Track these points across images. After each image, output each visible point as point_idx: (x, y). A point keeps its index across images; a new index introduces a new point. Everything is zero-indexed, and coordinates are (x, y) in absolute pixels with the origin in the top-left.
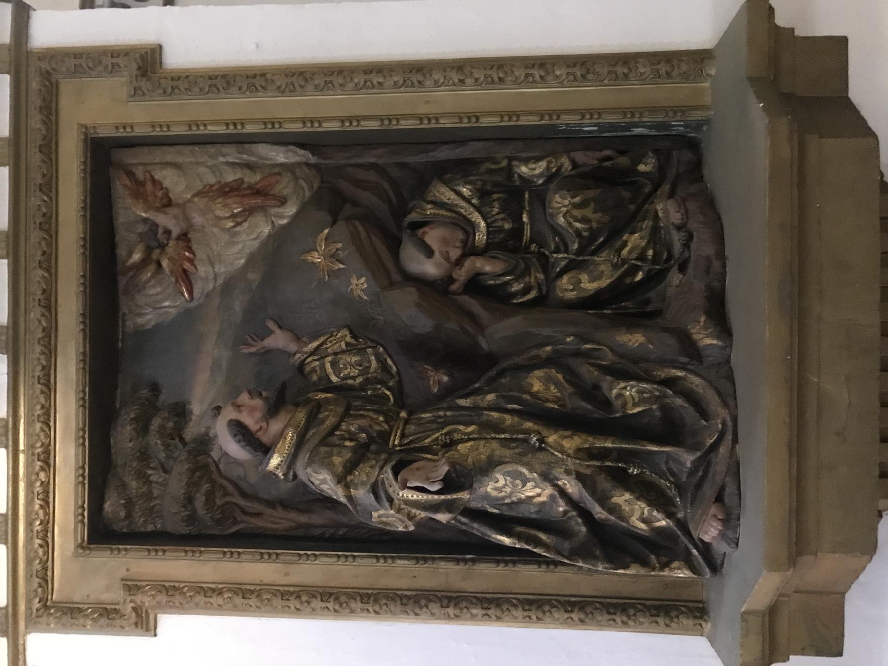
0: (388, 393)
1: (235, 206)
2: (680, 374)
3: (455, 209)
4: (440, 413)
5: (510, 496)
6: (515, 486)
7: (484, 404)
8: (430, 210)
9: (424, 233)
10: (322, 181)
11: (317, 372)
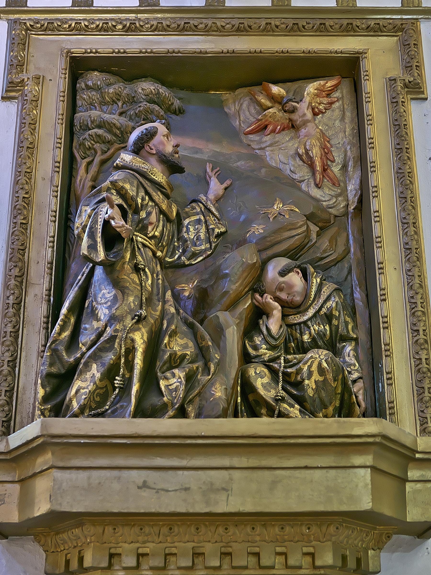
0: (176, 257)
4: (160, 276)
6: (106, 303)
8: (316, 281)
10: (336, 216)
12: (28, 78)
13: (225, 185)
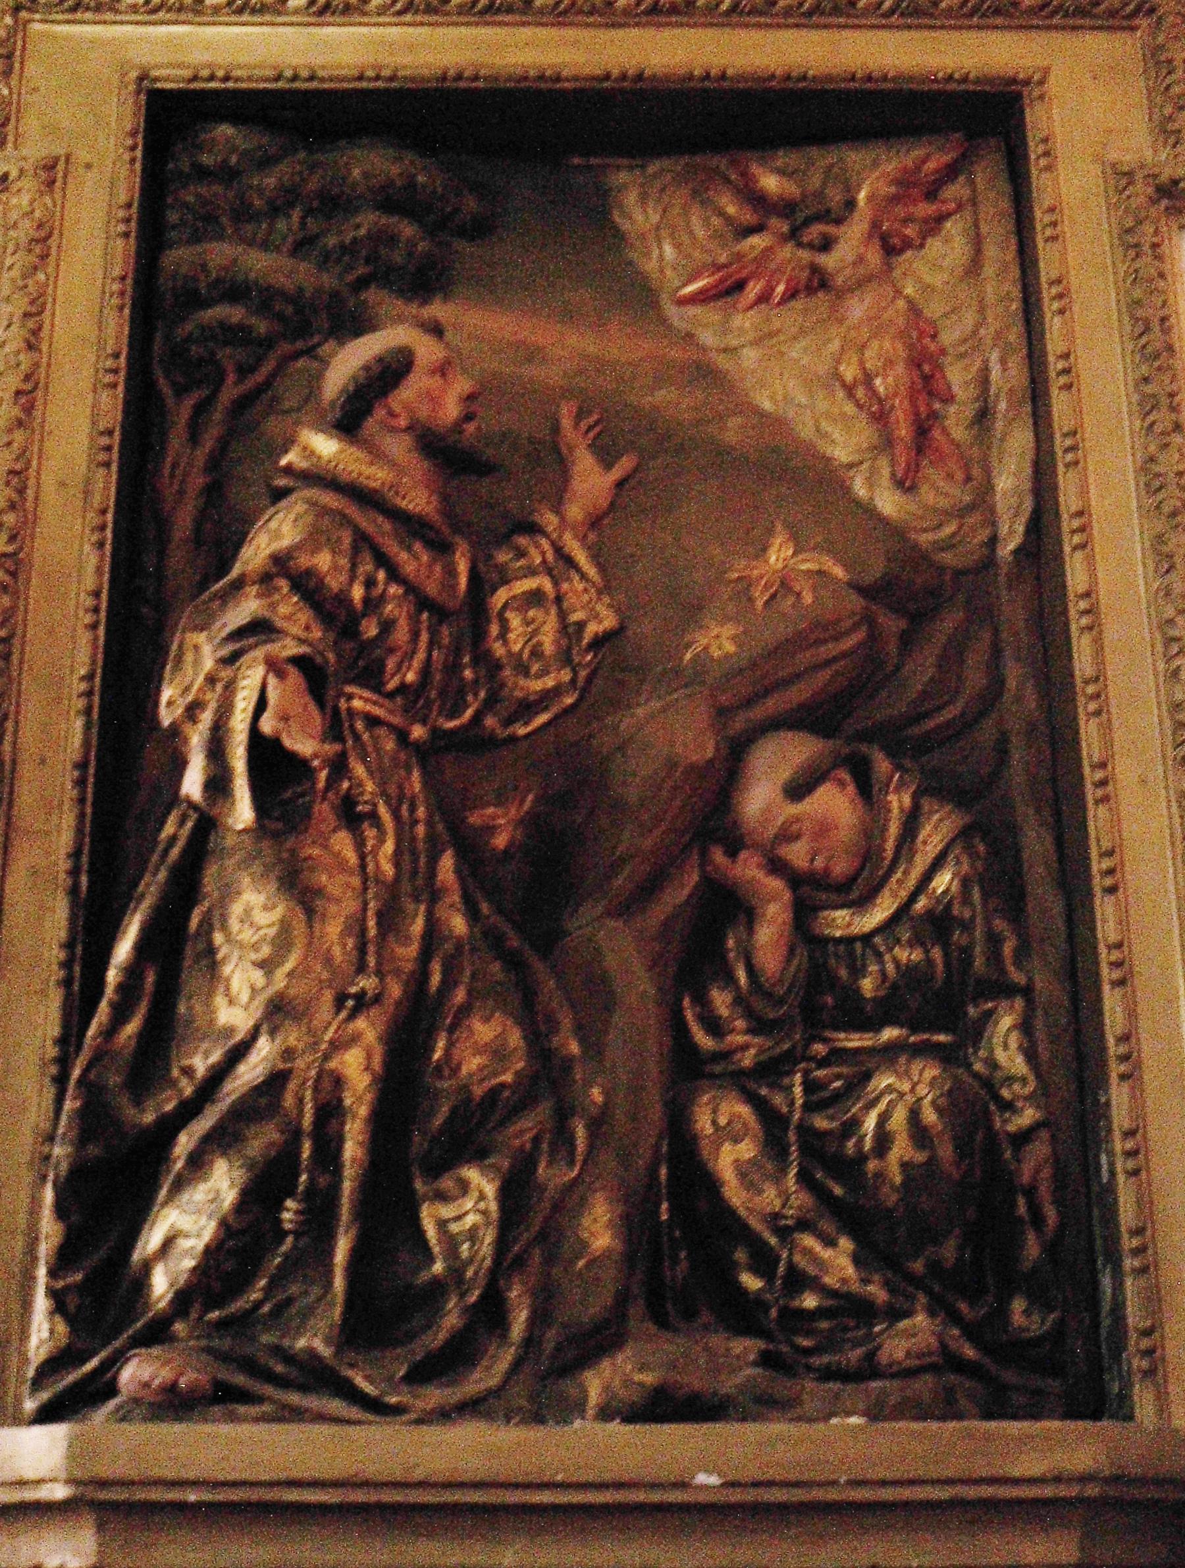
0: (469, 713)
1: (890, 379)
2: (517, 1329)
4: (422, 809)
5: (229, 939)
6: (255, 947)
7: (441, 912)
8: (898, 802)
9: (842, 784)
10: (958, 573)
11: (518, 560)
12: (22, 171)
13: (616, 473)
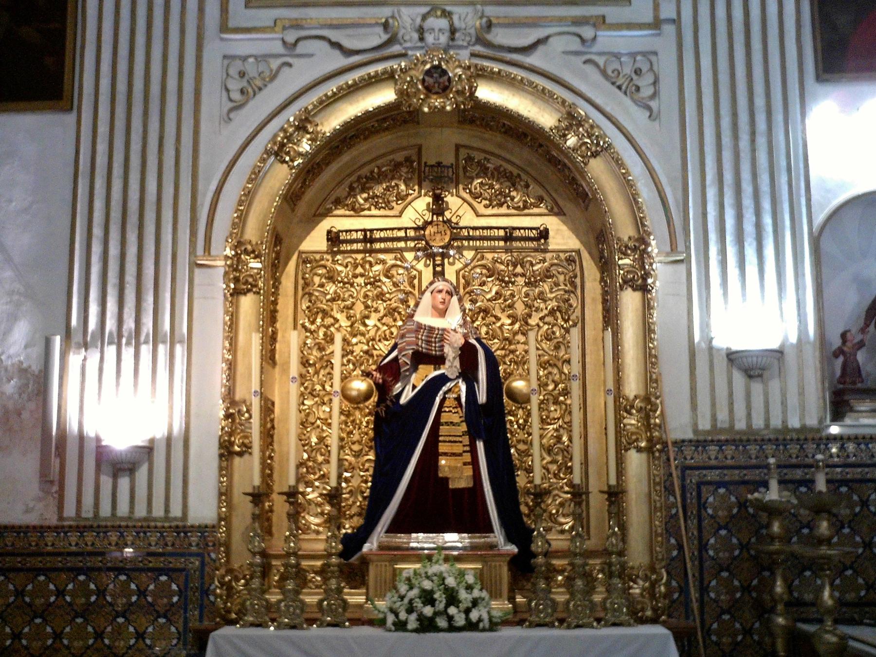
3: (702, 510)
